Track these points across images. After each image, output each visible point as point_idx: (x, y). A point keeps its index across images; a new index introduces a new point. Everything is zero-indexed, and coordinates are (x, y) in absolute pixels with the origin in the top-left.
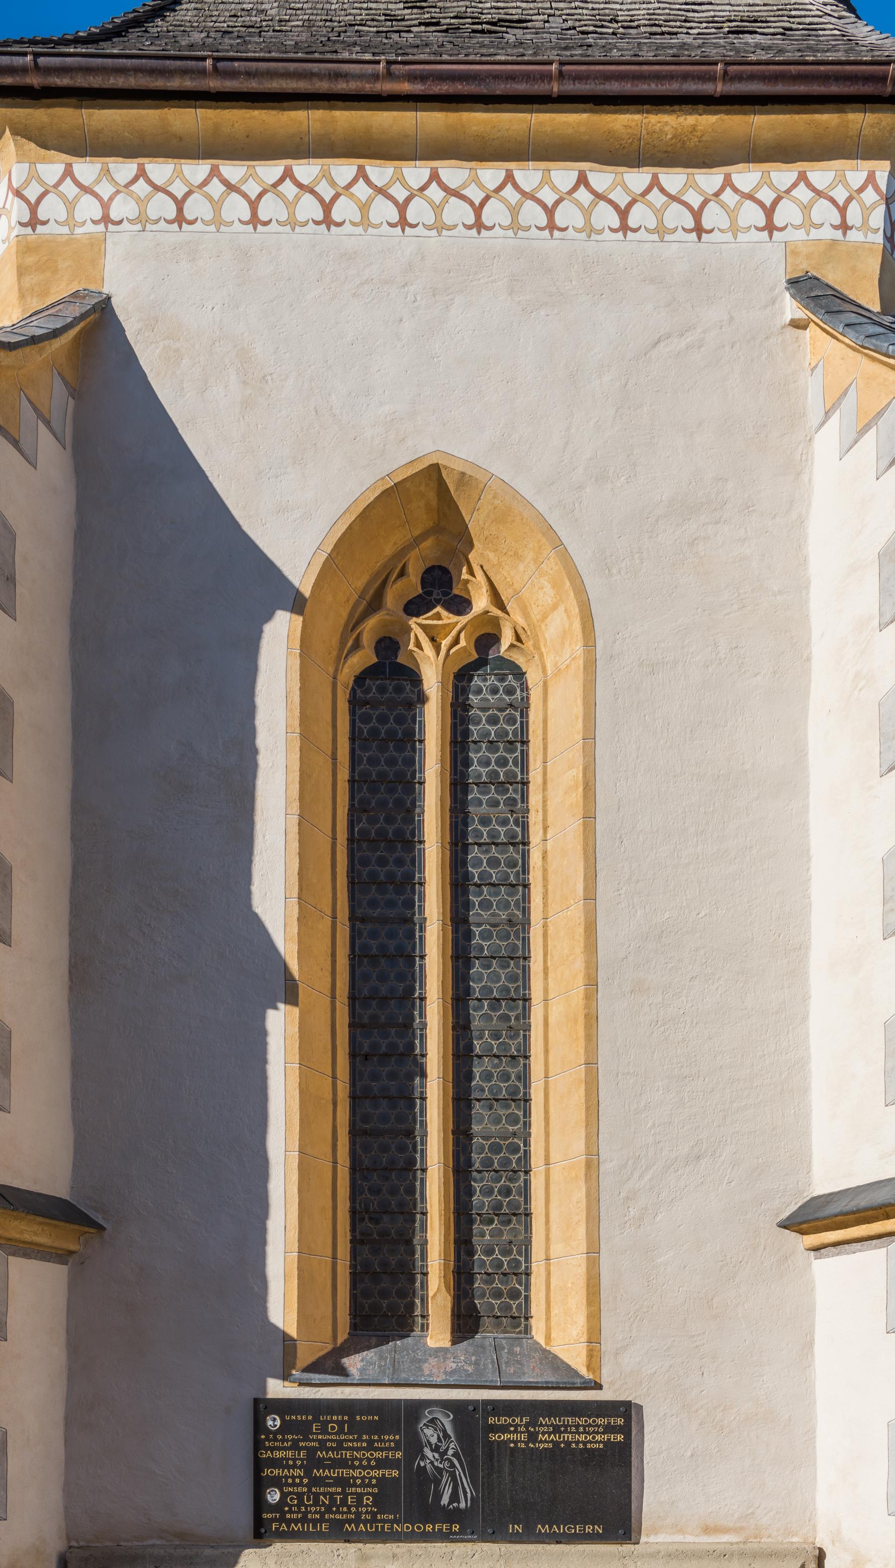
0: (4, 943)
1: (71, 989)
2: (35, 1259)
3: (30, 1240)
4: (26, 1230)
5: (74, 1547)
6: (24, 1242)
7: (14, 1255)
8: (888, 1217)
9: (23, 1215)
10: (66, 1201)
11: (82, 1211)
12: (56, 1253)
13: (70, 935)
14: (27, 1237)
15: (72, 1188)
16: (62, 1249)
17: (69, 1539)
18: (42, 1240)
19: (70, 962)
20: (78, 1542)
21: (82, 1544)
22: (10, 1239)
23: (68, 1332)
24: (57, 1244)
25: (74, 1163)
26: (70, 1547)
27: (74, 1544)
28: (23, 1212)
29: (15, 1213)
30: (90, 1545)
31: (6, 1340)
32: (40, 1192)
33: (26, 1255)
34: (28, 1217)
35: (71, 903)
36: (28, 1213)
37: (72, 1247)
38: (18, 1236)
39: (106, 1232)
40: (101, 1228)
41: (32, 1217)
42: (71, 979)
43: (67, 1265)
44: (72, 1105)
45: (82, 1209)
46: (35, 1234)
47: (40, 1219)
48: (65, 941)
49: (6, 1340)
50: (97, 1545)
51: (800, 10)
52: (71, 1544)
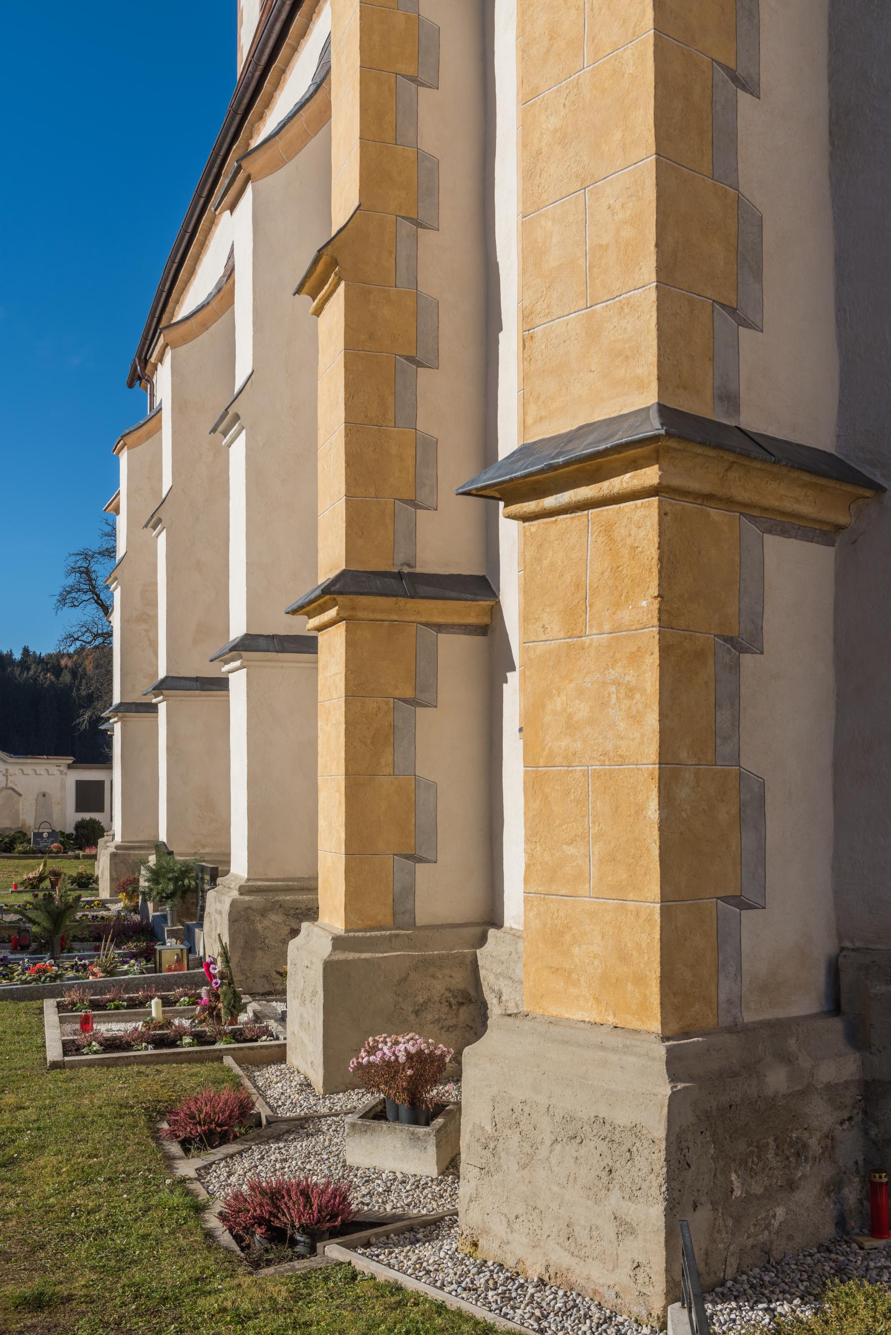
0: (752, 94)
1: (832, 156)
2: (796, 538)
3: (791, 510)
4: (786, 496)
5: (848, 949)
6: (783, 513)
7: (770, 532)
8: (674, 1333)
9: (785, 470)
10: (831, 455)
11: (853, 467)
12: (820, 530)
13: (829, 81)
14: (788, 505)
15: (839, 436)
16: (827, 523)
17: (840, 937)
18: (806, 509)
19: (830, 118)
20: (852, 942)
21: (858, 944)
22: (766, 509)
23: (835, 640)
24: (824, 515)
25: (840, 402)
26: (842, 949)
27: (847, 944)
28: (786, 465)
29: (775, 469)
30: (870, 946)
31: (762, 653)
32: (800, 442)
33: (784, 533)
34: (792, 474)
35: (830, 35)
36: (792, 467)
37: (842, 520)
38: (776, 504)
39: (887, 494)
40: (879, 489)
41: (795, 474)
42: (832, 144)
43: (833, 546)
44: (837, 319)
45: (853, 465)
46: (797, 501)
47: (806, 477)
48: (824, 89)
49: (762, 653)
50: (879, 947)
51: (220, 696)
52: (843, 945)
